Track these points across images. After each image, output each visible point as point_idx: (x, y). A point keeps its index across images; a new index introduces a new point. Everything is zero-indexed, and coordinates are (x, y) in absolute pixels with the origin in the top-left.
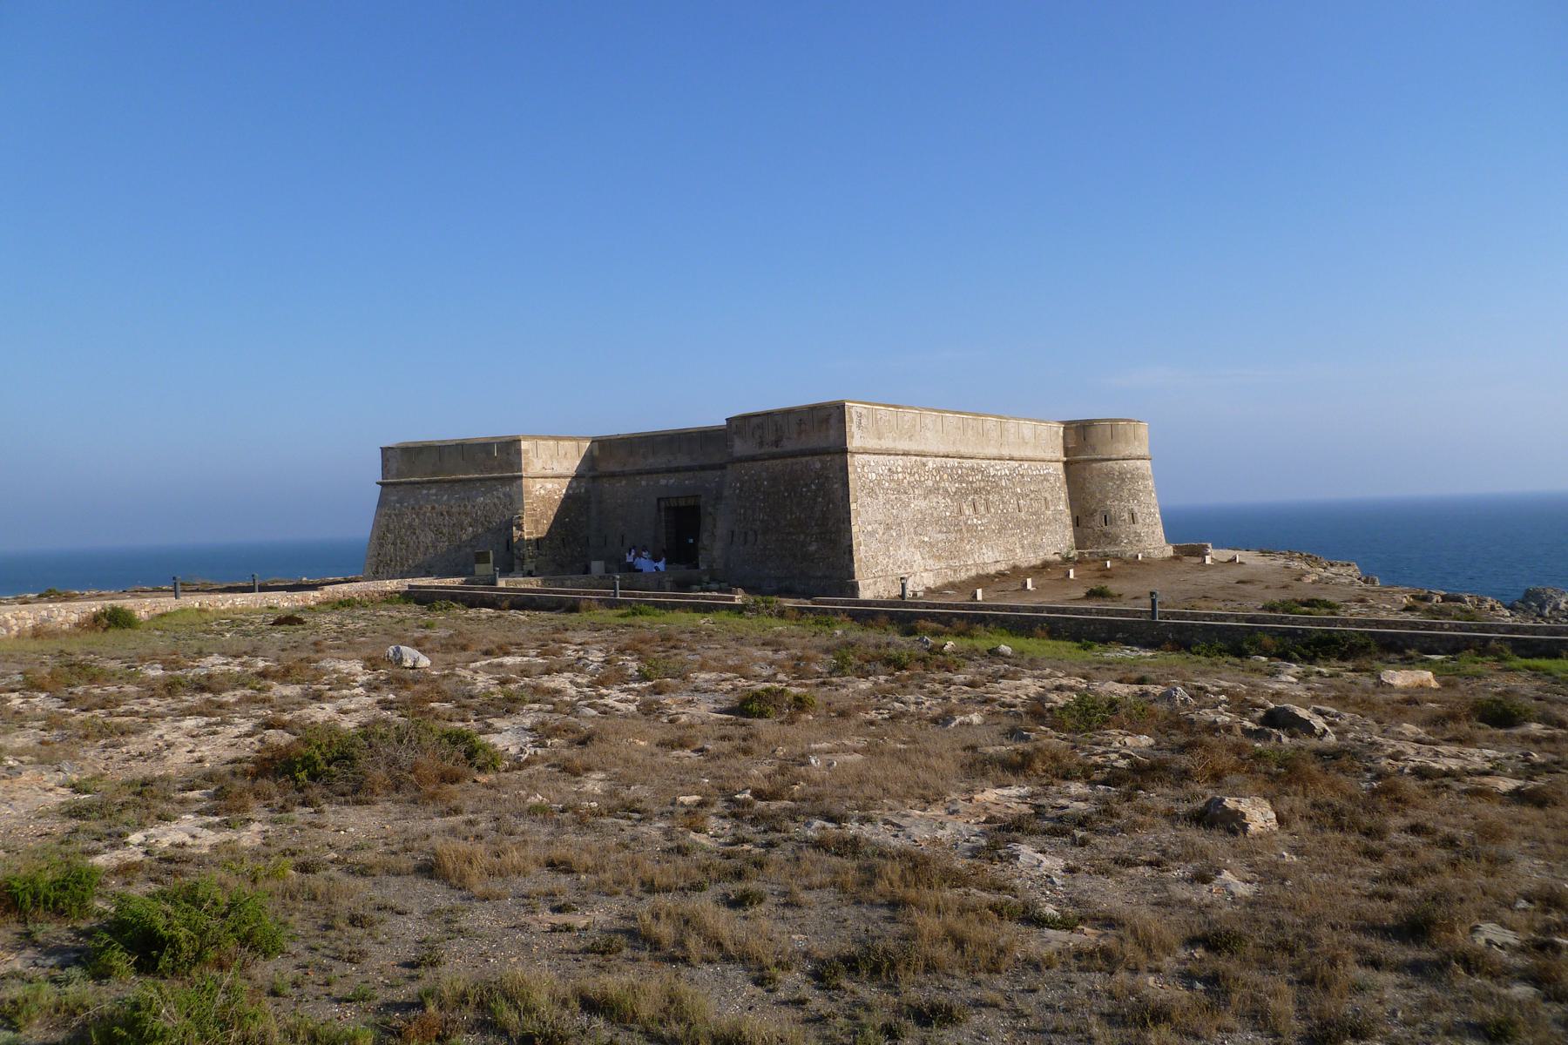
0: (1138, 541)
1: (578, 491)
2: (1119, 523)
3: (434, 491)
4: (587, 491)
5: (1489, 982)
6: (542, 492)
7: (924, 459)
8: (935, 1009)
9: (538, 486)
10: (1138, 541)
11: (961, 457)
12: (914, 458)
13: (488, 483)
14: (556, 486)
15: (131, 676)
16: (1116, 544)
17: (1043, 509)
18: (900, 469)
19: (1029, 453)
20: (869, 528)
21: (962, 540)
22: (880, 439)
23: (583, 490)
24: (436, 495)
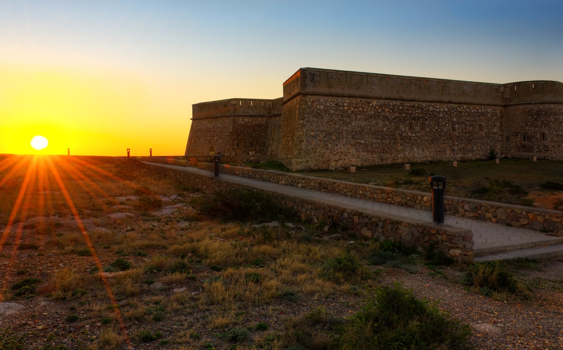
0: (545, 150)
1: (261, 122)
2: (533, 140)
3: (206, 122)
4: (266, 123)
5: (336, 285)
6: (243, 122)
7: (369, 100)
8: (83, 255)
9: (241, 120)
10: (545, 150)
11: (403, 100)
12: (359, 100)
13: (223, 118)
14: (251, 120)
15: (551, 216)
16: (530, 152)
17: (477, 130)
18: (346, 104)
19: (469, 99)
20: (313, 134)
21: (395, 144)
22: (329, 88)
23: (264, 122)
24: (207, 124)
